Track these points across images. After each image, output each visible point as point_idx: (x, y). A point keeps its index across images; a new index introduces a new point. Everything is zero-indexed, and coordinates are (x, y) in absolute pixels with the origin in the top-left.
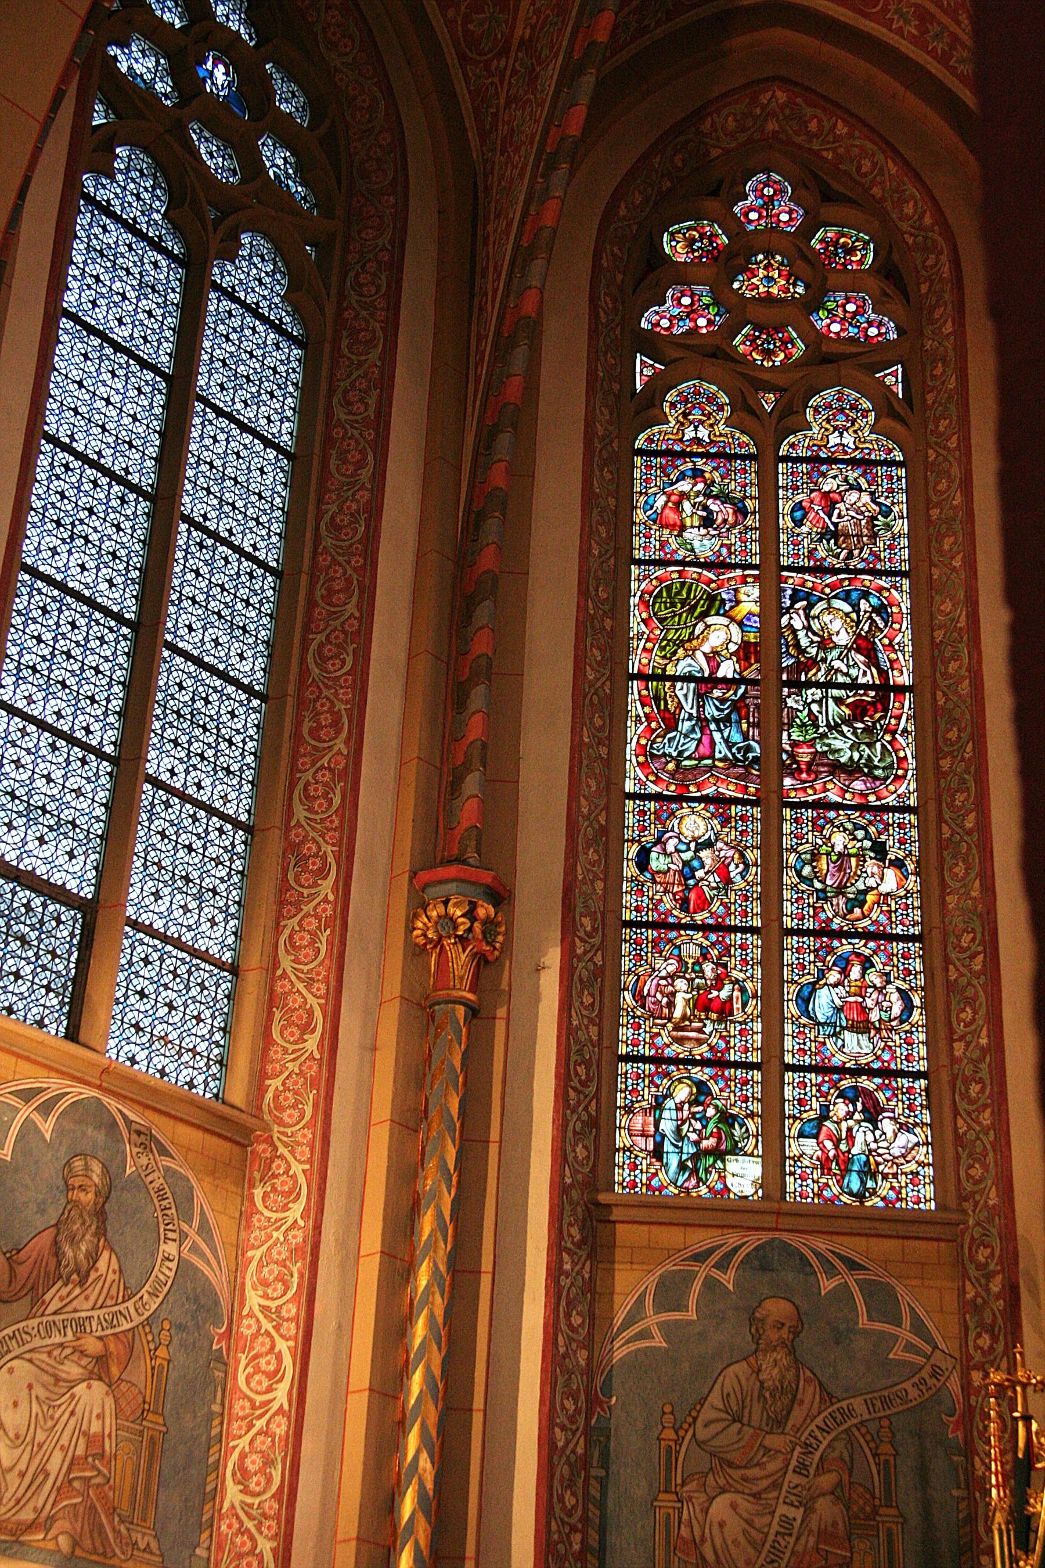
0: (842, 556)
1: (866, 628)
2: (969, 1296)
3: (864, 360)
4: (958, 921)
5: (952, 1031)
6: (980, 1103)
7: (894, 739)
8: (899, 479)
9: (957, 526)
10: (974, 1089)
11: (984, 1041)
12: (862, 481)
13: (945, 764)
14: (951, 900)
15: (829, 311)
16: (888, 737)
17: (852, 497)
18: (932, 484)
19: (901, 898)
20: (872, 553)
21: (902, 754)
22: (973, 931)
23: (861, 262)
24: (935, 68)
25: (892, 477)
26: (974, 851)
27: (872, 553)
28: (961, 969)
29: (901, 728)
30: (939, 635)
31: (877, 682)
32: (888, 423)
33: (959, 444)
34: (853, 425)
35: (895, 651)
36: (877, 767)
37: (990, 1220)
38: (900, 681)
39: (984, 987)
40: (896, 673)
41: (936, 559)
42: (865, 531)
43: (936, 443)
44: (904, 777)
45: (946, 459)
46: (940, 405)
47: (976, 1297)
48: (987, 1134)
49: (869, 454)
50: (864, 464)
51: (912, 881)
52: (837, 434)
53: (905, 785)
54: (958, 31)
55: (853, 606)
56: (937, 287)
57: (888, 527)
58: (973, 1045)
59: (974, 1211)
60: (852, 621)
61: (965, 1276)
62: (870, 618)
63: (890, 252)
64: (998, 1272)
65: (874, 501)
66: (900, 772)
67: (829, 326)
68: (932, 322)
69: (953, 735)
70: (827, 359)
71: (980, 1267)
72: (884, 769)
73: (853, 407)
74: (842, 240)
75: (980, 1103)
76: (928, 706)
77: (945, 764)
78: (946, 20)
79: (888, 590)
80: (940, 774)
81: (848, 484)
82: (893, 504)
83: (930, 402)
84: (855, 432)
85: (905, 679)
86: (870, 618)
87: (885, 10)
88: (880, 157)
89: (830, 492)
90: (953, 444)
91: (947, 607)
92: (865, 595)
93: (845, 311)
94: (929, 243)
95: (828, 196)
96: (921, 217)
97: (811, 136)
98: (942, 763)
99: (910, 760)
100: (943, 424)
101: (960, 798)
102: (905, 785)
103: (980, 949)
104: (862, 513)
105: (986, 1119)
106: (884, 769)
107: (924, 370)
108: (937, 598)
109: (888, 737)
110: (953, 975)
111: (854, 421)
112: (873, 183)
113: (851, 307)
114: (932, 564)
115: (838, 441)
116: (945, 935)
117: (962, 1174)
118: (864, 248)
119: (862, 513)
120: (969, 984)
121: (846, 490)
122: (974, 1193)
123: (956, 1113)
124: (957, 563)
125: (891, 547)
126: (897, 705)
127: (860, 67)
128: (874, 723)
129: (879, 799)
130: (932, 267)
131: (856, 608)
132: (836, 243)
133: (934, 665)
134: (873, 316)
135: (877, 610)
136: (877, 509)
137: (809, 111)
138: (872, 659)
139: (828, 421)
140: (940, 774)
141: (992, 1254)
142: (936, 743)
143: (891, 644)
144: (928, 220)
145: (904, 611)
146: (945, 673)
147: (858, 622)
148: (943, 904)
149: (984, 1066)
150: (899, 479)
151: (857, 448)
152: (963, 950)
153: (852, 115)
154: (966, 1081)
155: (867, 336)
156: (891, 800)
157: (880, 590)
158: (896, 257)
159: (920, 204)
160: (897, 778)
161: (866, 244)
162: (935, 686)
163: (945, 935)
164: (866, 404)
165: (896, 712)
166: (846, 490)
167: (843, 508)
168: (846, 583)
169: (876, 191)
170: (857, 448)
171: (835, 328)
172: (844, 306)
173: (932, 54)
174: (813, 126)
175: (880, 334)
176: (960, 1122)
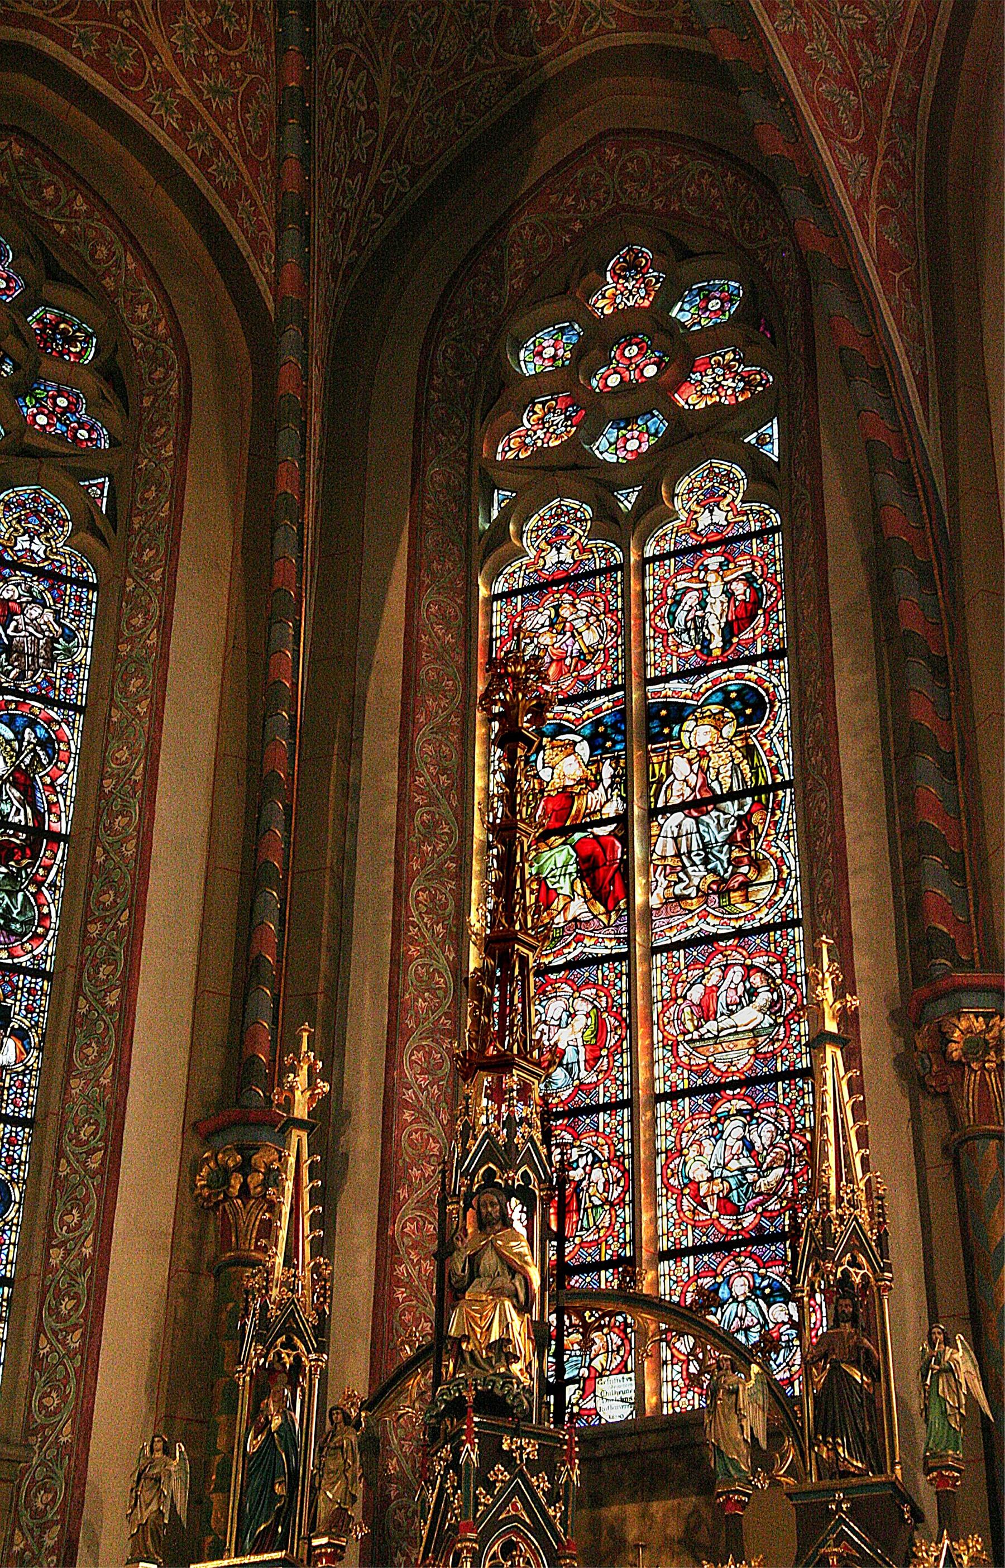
0: (12, 676)
1: (27, 761)
2: (15, 1549)
3: (70, 463)
4: (79, 1109)
5: (51, 1235)
6: (73, 1320)
7: (39, 892)
8: (89, 603)
9: (148, 668)
10: (67, 1305)
11: (87, 1251)
12: (48, 596)
13: (94, 929)
14: (76, 1085)
15: (38, 400)
16: (33, 889)
17: (35, 612)
18: (126, 617)
19: (18, 1074)
20: (46, 678)
21: (45, 910)
22: (96, 1123)
23: (79, 355)
24: (192, 171)
25: (81, 599)
26: (112, 1032)
27: (46, 678)
28: (75, 1165)
29: (49, 881)
30: (109, 784)
31: (31, 824)
32: (86, 538)
33: (163, 579)
34: (46, 531)
35: (56, 793)
36: (15, 921)
37: (58, 1459)
38: (56, 827)
39: (98, 1189)
40: (53, 818)
41: (118, 697)
42: (43, 653)
43: (139, 575)
44: (44, 936)
45: (146, 593)
46: (148, 531)
47: (24, 1551)
48: (72, 1359)
49: (60, 568)
50: (53, 578)
51: (32, 1059)
52: (26, 537)
53: (43, 946)
54: (223, 138)
55: (15, 734)
56: (161, 403)
57: (69, 653)
58: (74, 1253)
59: (41, 1448)
60: (13, 749)
61: (17, 1523)
62: (33, 750)
63: (116, 350)
64: (57, 1523)
65: (57, 621)
66: (40, 930)
67: (34, 416)
68: (150, 440)
69: (108, 898)
70: (28, 453)
71: (36, 1514)
72: (22, 923)
73: (49, 512)
74: (62, 326)
75: (73, 1320)
76: (84, 861)
77: (94, 929)
78: (212, 123)
79: (58, 723)
80: (85, 939)
81: (32, 596)
82: (78, 628)
83: (136, 526)
84: (48, 540)
85: (62, 827)
86: (33, 750)
87: (146, 91)
88: (119, 247)
89: (9, 600)
90: (156, 577)
91: (124, 755)
92: (32, 724)
93: (55, 404)
94: (160, 353)
95: (54, 274)
96: (156, 324)
97: (45, 203)
98: (91, 928)
99: (53, 920)
100: (148, 554)
101: (104, 970)
102: (43, 946)
103: (101, 1144)
104: (42, 632)
105: (74, 1340)
106: (22, 923)
107: (134, 491)
108: (114, 744)
109: (33, 889)
110: (64, 1170)
111: (48, 527)
112: (107, 273)
113: (62, 402)
114: (112, 704)
115: (26, 545)
116: (63, 1123)
117: (35, 1404)
118: (85, 341)
119: (42, 632)
120: (82, 1183)
121: (29, 603)
122: (44, 1427)
123: (40, 1330)
124: (142, 709)
125: (68, 676)
126: (48, 853)
127: (110, 144)
128: (19, 870)
129: (11, 956)
130: (159, 381)
131: (19, 736)
132: (55, 328)
133: (99, 815)
134: (85, 418)
135: (41, 743)
136: (60, 631)
137: (46, 176)
138: (29, 798)
139: (19, 522)
140: (85, 939)
141: (54, 1500)
142: (87, 905)
143: (52, 785)
144: (161, 329)
145: (73, 750)
146: (111, 828)
147: (19, 753)
148: (66, 1087)
149: (83, 1280)
150: (89, 603)
151: (47, 559)
152: (80, 1144)
153: (95, 194)
154: (59, 1297)
155: (75, 437)
156: (24, 960)
157: (50, 721)
158: (119, 359)
159: (156, 309)
160: (36, 936)
161: (89, 337)
162: (96, 841)
163: (63, 1123)
164: (65, 513)
165: (48, 862)
166: (28, 602)
167: (21, 621)
168: (13, 706)
169: (109, 282)
170: (47, 559)
171: (42, 420)
172: (54, 398)
173: (192, 153)
174: (49, 193)
175: (90, 439)
176: (43, 1342)
